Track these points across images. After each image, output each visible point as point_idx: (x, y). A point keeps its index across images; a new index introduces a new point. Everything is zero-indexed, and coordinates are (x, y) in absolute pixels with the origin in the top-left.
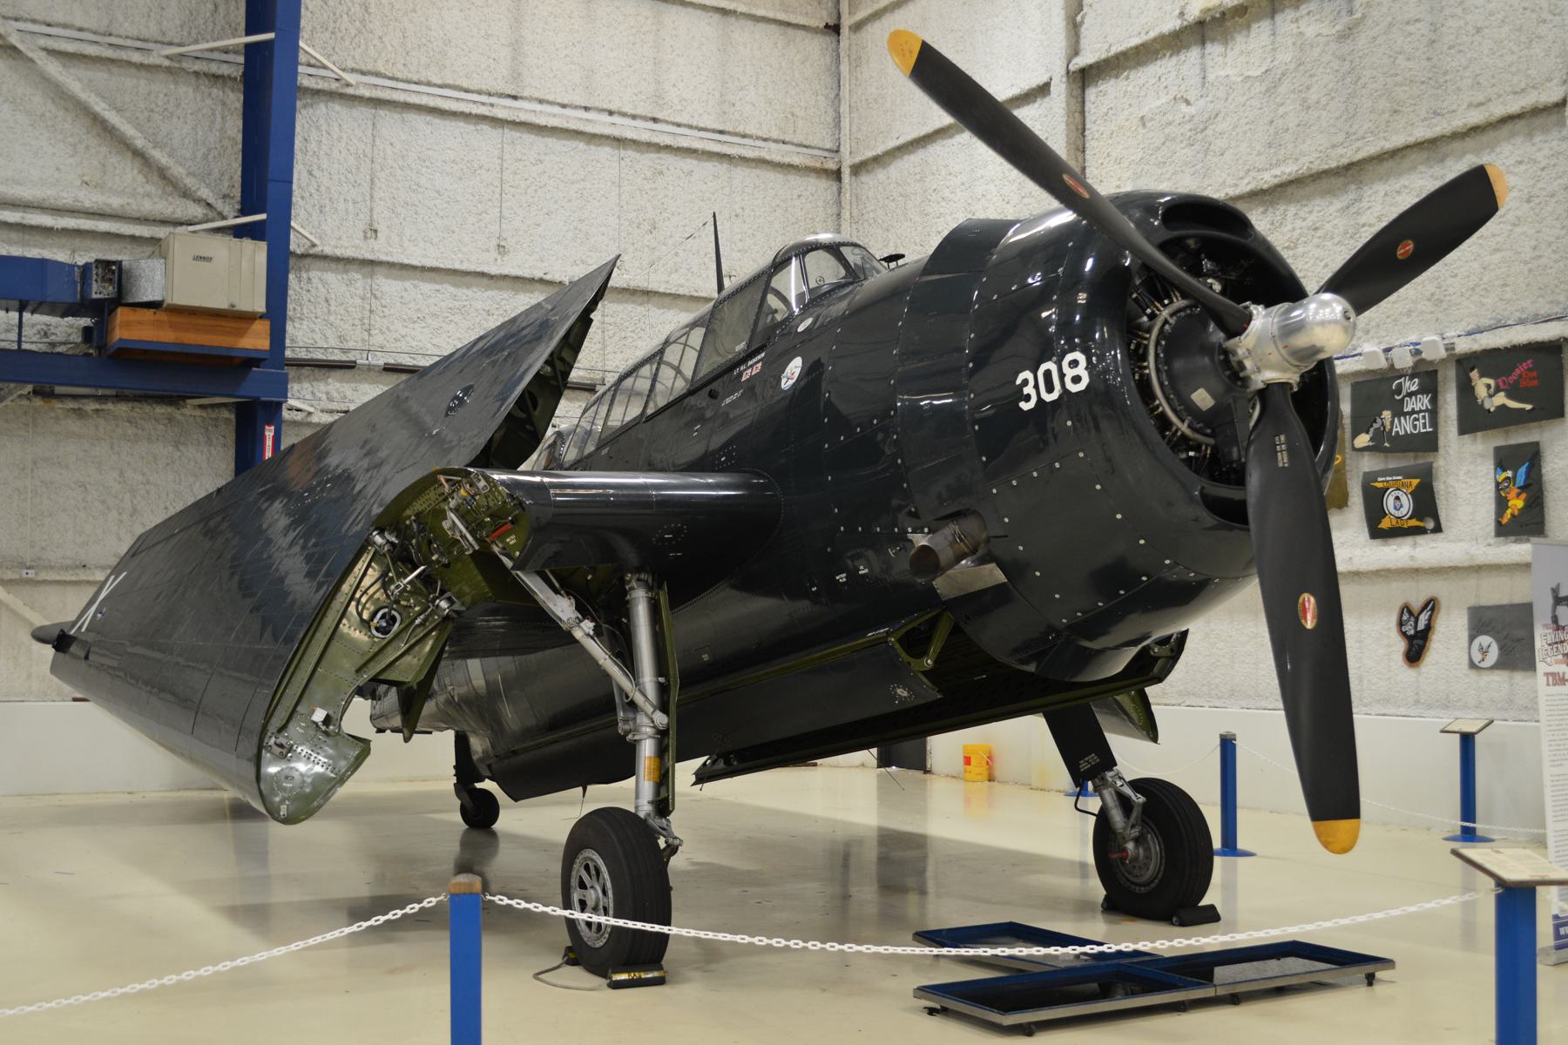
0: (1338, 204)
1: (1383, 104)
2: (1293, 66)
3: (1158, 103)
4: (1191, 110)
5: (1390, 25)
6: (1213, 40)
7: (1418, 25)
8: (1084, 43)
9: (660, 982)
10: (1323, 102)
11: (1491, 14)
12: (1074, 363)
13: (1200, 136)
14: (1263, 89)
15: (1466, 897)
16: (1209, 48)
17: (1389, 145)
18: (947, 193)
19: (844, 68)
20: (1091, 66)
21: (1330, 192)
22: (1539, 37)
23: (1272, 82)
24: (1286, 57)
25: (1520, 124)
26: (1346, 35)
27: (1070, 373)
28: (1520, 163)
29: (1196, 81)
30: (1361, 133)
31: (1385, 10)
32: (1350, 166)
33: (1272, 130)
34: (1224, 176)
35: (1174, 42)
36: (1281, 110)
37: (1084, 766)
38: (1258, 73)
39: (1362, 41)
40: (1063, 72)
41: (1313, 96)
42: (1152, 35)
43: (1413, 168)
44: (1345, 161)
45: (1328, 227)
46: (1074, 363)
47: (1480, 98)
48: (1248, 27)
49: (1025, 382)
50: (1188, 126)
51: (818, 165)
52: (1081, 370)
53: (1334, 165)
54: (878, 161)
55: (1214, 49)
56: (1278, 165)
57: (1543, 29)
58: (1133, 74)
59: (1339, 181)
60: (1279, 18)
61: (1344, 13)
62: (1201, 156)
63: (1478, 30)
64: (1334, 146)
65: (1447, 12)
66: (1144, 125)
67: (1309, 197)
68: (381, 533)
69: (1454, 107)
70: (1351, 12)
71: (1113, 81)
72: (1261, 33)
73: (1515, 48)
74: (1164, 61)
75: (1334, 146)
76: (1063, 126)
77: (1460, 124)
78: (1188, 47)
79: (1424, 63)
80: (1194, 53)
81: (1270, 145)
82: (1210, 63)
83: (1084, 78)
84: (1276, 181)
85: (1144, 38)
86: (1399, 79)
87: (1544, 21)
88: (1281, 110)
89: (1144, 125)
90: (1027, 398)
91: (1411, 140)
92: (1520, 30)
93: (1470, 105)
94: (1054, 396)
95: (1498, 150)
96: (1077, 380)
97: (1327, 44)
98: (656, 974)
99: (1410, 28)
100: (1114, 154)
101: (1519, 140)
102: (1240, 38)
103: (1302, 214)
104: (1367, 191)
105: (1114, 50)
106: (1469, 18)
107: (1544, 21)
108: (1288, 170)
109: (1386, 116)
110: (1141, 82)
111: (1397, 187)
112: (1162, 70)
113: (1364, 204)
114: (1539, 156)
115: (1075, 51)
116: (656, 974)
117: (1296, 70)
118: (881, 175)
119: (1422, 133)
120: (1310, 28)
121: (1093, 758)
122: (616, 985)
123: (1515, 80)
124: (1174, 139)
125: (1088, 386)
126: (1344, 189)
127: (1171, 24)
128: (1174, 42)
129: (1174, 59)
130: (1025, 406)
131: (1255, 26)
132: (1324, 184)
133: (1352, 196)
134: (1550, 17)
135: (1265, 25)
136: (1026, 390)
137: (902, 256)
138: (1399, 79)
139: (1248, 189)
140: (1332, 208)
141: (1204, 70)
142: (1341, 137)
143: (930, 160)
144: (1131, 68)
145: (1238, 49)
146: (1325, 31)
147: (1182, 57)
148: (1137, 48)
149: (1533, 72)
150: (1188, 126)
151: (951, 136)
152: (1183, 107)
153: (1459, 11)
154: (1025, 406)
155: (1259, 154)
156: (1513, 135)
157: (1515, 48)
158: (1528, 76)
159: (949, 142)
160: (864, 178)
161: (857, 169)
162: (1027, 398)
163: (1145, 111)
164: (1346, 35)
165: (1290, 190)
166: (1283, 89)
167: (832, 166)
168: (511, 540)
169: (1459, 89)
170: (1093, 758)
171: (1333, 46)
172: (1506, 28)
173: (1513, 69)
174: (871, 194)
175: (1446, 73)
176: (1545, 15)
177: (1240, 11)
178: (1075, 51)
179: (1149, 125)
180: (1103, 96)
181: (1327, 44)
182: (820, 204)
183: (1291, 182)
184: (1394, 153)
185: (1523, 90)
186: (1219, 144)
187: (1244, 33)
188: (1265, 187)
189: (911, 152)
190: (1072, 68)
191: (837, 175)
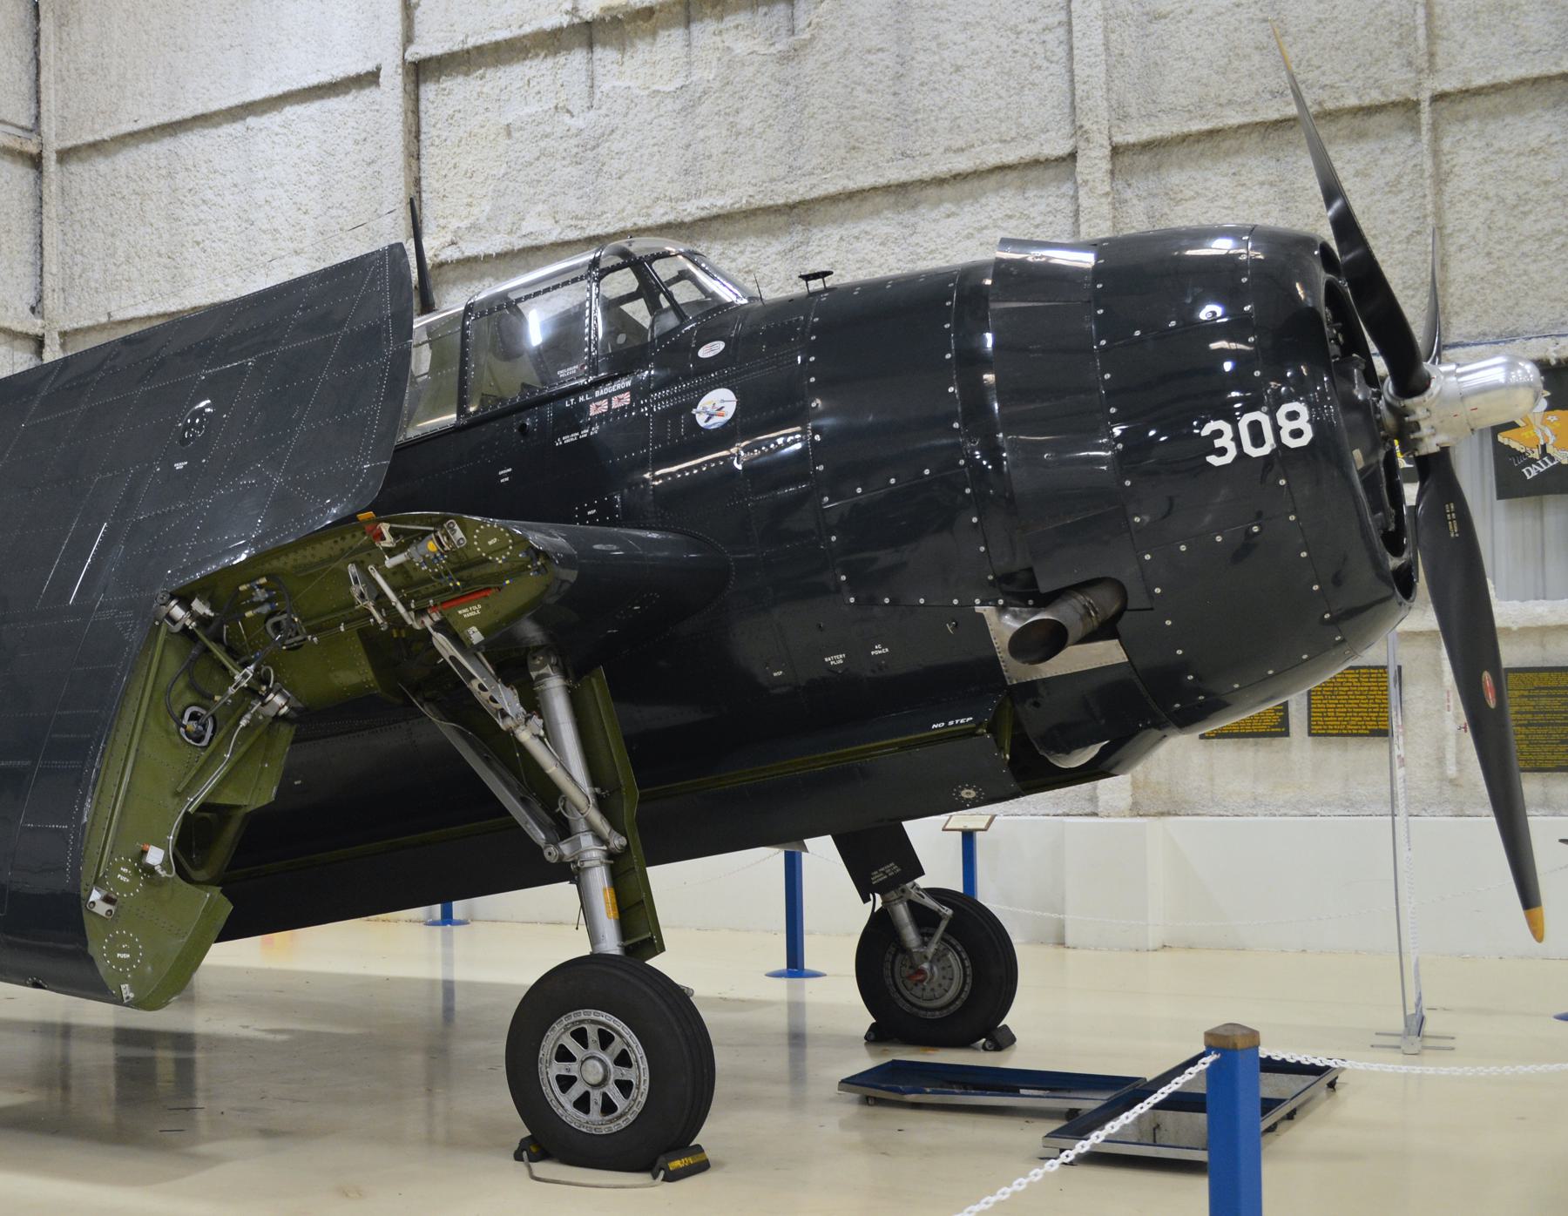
0: (777, 246)
1: (837, 137)
2: (716, 85)
3: (528, 110)
4: (578, 122)
5: (846, 51)
6: (604, 45)
7: (880, 55)
8: (419, 29)
9: (703, 1166)
10: (758, 129)
11: (975, 52)
12: (1293, 416)
13: (590, 154)
14: (678, 106)
15: (165, 1019)
16: (599, 52)
17: (851, 186)
18: (209, 195)
19: (47, 25)
20: (430, 59)
21: (769, 231)
22: (1033, 84)
23: (689, 102)
24: (705, 74)
25: (1011, 176)
26: (789, 57)
27: (1287, 426)
28: (1010, 217)
29: (581, 88)
30: (808, 167)
31: (839, 33)
32: (791, 208)
33: (689, 154)
34: (623, 203)
35: (551, 42)
36: (701, 134)
37: (877, 877)
38: (671, 87)
39: (810, 65)
40: (399, 62)
41: (744, 121)
42: (527, 29)
43: (876, 212)
44: (795, 198)
45: (765, 270)
46: (1293, 416)
47: (960, 143)
48: (654, 34)
49: (1218, 434)
50: (574, 141)
51: (18, 146)
52: (1302, 422)
53: (781, 201)
54: (97, 147)
55: (605, 56)
56: (698, 195)
57: (1036, 76)
58: (490, 73)
59: (782, 220)
60: (696, 28)
61: (783, 31)
62: (591, 177)
63: (958, 69)
64: (772, 180)
65: (918, 44)
66: (509, 135)
67: (740, 235)
68: (185, 603)
69: (928, 150)
70: (792, 32)
71: (460, 79)
72: (670, 43)
73: (1003, 93)
74: (536, 62)
75: (772, 180)
76: (399, 126)
77: (945, 169)
78: (569, 49)
79: (891, 98)
80: (578, 57)
81: (687, 172)
82: (599, 70)
83: (420, 72)
84: (703, 214)
85: (514, 32)
86: (857, 112)
87: (1039, 68)
88: (701, 134)
89: (509, 135)
90: (1222, 452)
91: (882, 181)
92: (1009, 73)
93: (947, 150)
94: (1265, 450)
95: (983, 201)
96: (1297, 434)
97: (763, 64)
98: (690, 1160)
99: (871, 58)
100: (463, 166)
101: (1009, 193)
102: (642, 46)
103: (730, 253)
104: (816, 234)
105: (471, 43)
106: (946, 54)
107: (1039, 68)
108: (720, 203)
109: (842, 152)
110: (503, 83)
111: (856, 232)
112: (533, 72)
113: (813, 247)
114: (1033, 212)
115: (408, 39)
116: (690, 1160)
117: (722, 89)
118: (102, 165)
119: (894, 174)
120: (741, 47)
121: (892, 868)
122: (672, 1177)
123: (1003, 128)
124: (552, 155)
125: (1312, 442)
126: (787, 228)
127: (556, 19)
128: (551, 42)
129: (550, 62)
130: (1214, 460)
131: (663, 34)
132: (761, 222)
133: (797, 238)
134: (1046, 64)
135: (678, 34)
136: (1218, 443)
137: (829, 273)
138: (857, 112)
139: (664, 220)
140: (770, 250)
141: (592, 77)
142: (781, 170)
143: (183, 152)
144: (487, 66)
145: (639, 57)
146: (763, 50)
147: (561, 59)
148: (497, 43)
149: (1027, 121)
150: (574, 141)
151: (218, 125)
152: (567, 117)
153: (933, 46)
154: (1214, 460)
155: (672, 181)
156: (1001, 186)
157: (1003, 93)
158: (1019, 125)
159: (213, 132)
160: (74, 167)
161: (64, 156)
162: (1222, 452)
163: (510, 117)
164: (789, 57)
165: (715, 225)
166: (703, 110)
167: (32, 148)
168: (469, 612)
169: (934, 131)
170: (892, 868)
171: (772, 68)
172: (992, 70)
173: (1001, 115)
174: (85, 189)
175: (917, 111)
176: (1039, 61)
177: (648, 13)
178: (408, 39)
179: (516, 135)
180: (440, 97)
181: (763, 64)
182: (15, 195)
183: (717, 217)
184: (850, 196)
185: (1013, 139)
186: (616, 165)
187: (649, 40)
188: (688, 219)
189: (151, 141)
190: (409, 58)
191: (36, 162)
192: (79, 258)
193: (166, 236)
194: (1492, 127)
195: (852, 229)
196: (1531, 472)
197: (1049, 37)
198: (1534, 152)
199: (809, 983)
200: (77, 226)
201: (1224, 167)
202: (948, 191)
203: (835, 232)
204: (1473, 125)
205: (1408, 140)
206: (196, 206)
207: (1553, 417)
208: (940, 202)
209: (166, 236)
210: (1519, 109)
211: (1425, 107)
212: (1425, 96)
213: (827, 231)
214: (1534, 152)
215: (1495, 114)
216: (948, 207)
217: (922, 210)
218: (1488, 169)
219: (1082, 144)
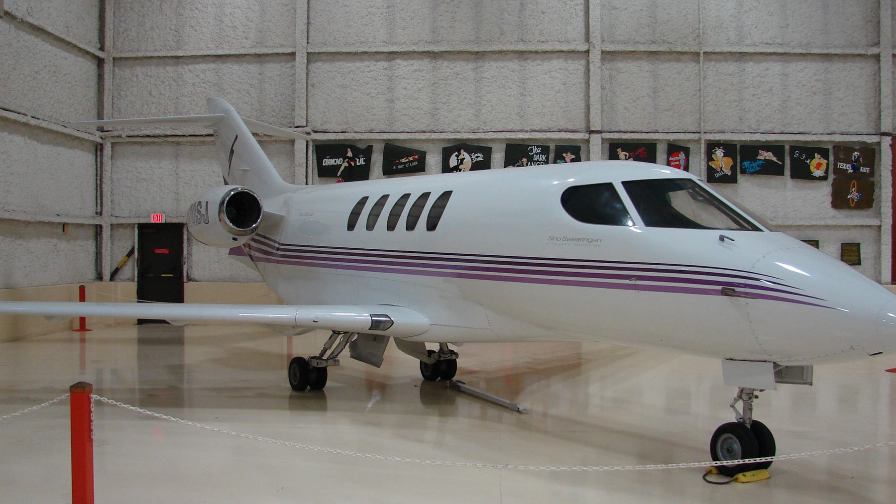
18: (200, 6)
21: (467, 60)
25: (563, 54)
43: (511, 60)
47: (543, 39)
63: (544, 13)
119: (521, 47)
156: (558, 58)
161: (608, 55)
192: (123, 25)
193: (174, 22)
194: (718, 65)
195: (500, 64)
196: (717, 175)
197: (577, 7)
198: (731, 75)
199: (87, 333)
200: (122, 10)
201: (635, 63)
202: (538, 56)
203: (494, 64)
204: (713, 63)
205: (694, 64)
206: (192, 10)
207: (725, 159)
208: (535, 60)
209: (174, 22)
210: (726, 60)
211: (702, 55)
212: (702, 52)
213: (491, 63)
214: (731, 75)
215: (719, 61)
216: (539, 62)
217: (529, 61)
218: (716, 78)
219: (591, 48)
